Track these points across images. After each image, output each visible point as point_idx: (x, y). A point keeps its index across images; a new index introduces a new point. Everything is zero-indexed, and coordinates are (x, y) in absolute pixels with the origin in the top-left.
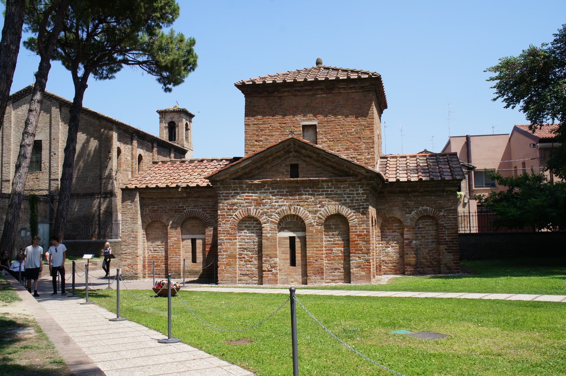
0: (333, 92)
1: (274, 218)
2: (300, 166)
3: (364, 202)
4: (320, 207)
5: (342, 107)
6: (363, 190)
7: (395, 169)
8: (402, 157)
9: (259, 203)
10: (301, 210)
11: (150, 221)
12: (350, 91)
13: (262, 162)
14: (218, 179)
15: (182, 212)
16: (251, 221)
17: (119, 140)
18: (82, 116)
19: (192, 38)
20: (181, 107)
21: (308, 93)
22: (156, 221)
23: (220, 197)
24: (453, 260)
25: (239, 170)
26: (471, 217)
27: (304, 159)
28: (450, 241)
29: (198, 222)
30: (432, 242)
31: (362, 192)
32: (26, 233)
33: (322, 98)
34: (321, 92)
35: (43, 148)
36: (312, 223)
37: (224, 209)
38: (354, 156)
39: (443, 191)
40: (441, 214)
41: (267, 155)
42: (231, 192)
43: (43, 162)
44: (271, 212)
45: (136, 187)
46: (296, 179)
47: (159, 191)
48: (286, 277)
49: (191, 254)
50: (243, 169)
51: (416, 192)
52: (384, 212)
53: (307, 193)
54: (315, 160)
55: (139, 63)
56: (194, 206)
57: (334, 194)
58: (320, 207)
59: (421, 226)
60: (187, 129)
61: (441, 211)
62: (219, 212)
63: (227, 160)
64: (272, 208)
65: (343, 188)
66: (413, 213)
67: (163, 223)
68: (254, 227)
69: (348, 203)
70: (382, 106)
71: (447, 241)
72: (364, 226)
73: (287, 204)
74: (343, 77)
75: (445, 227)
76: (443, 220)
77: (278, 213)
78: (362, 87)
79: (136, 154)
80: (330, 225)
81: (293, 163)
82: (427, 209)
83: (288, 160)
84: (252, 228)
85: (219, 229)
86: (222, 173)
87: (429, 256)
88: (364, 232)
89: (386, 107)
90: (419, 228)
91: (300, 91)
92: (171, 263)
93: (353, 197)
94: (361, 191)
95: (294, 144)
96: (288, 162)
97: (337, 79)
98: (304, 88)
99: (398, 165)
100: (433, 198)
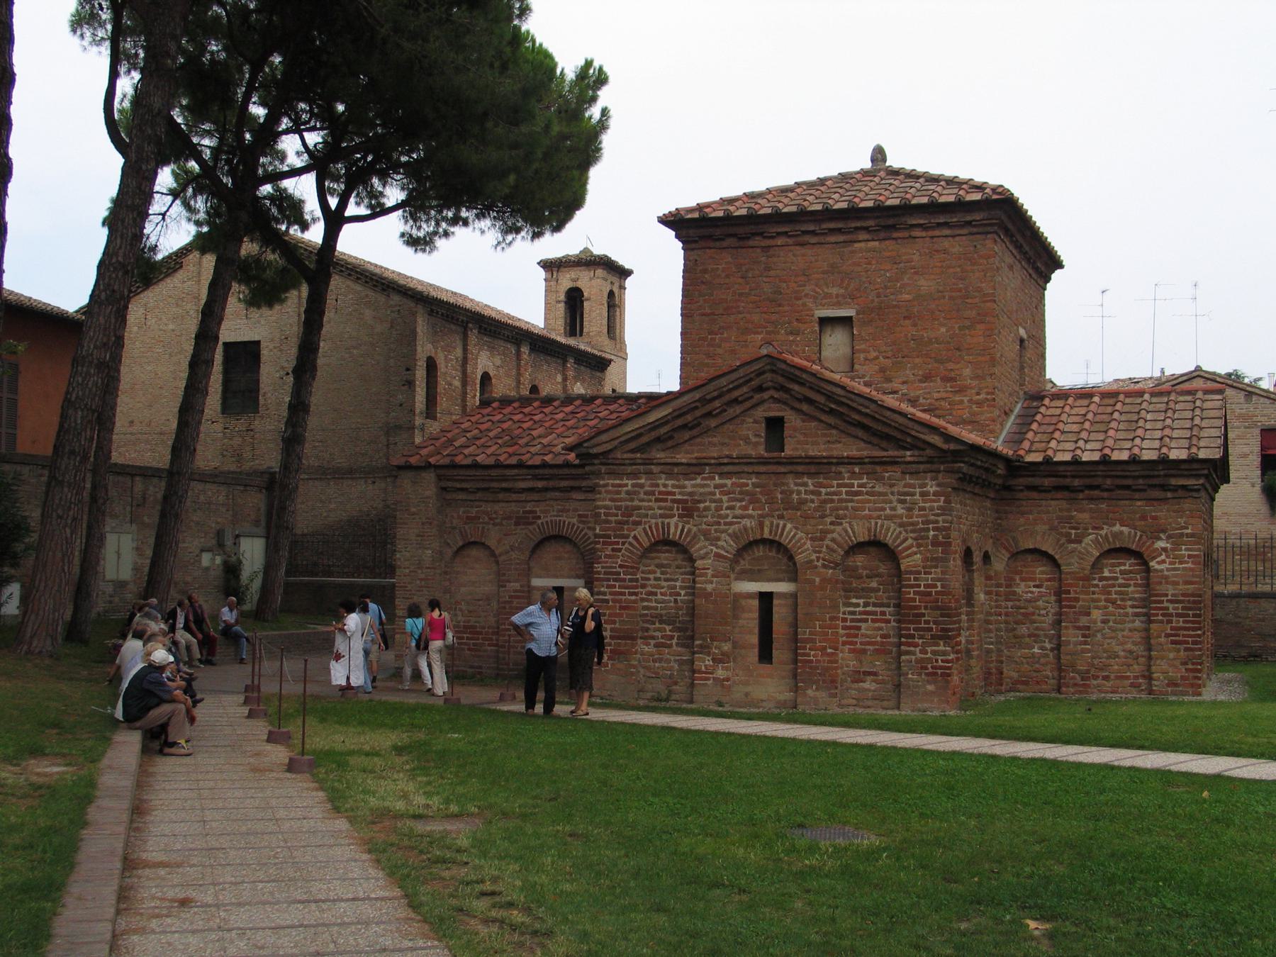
0: (895, 235)
3: (938, 515)
4: (832, 523)
5: (916, 273)
6: (938, 485)
9: (689, 510)
10: (787, 529)
11: (461, 544)
18: (337, 284)
20: (597, 251)
21: (832, 239)
23: (600, 493)
24: (1185, 663)
27: (797, 405)
28: (1178, 615)
29: (568, 547)
30: (1137, 615)
32: (213, 560)
33: (869, 250)
35: (263, 359)
36: (812, 561)
37: (607, 522)
38: (944, 395)
39: (1164, 487)
41: (708, 397)
42: (625, 481)
43: (261, 392)
46: (776, 454)
53: (802, 489)
56: (559, 511)
58: (832, 523)
61: (1160, 539)
64: (719, 523)
65: (889, 478)
67: (488, 548)
69: (901, 517)
71: (1171, 615)
72: (936, 572)
76: (1163, 562)
77: (734, 536)
78: (969, 223)
81: (772, 414)
83: (760, 409)
85: (598, 567)
88: (936, 586)
89: (1056, 263)
91: (813, 233)
94: (932, 488)
96: (761, 413)
100: (1139, 503)
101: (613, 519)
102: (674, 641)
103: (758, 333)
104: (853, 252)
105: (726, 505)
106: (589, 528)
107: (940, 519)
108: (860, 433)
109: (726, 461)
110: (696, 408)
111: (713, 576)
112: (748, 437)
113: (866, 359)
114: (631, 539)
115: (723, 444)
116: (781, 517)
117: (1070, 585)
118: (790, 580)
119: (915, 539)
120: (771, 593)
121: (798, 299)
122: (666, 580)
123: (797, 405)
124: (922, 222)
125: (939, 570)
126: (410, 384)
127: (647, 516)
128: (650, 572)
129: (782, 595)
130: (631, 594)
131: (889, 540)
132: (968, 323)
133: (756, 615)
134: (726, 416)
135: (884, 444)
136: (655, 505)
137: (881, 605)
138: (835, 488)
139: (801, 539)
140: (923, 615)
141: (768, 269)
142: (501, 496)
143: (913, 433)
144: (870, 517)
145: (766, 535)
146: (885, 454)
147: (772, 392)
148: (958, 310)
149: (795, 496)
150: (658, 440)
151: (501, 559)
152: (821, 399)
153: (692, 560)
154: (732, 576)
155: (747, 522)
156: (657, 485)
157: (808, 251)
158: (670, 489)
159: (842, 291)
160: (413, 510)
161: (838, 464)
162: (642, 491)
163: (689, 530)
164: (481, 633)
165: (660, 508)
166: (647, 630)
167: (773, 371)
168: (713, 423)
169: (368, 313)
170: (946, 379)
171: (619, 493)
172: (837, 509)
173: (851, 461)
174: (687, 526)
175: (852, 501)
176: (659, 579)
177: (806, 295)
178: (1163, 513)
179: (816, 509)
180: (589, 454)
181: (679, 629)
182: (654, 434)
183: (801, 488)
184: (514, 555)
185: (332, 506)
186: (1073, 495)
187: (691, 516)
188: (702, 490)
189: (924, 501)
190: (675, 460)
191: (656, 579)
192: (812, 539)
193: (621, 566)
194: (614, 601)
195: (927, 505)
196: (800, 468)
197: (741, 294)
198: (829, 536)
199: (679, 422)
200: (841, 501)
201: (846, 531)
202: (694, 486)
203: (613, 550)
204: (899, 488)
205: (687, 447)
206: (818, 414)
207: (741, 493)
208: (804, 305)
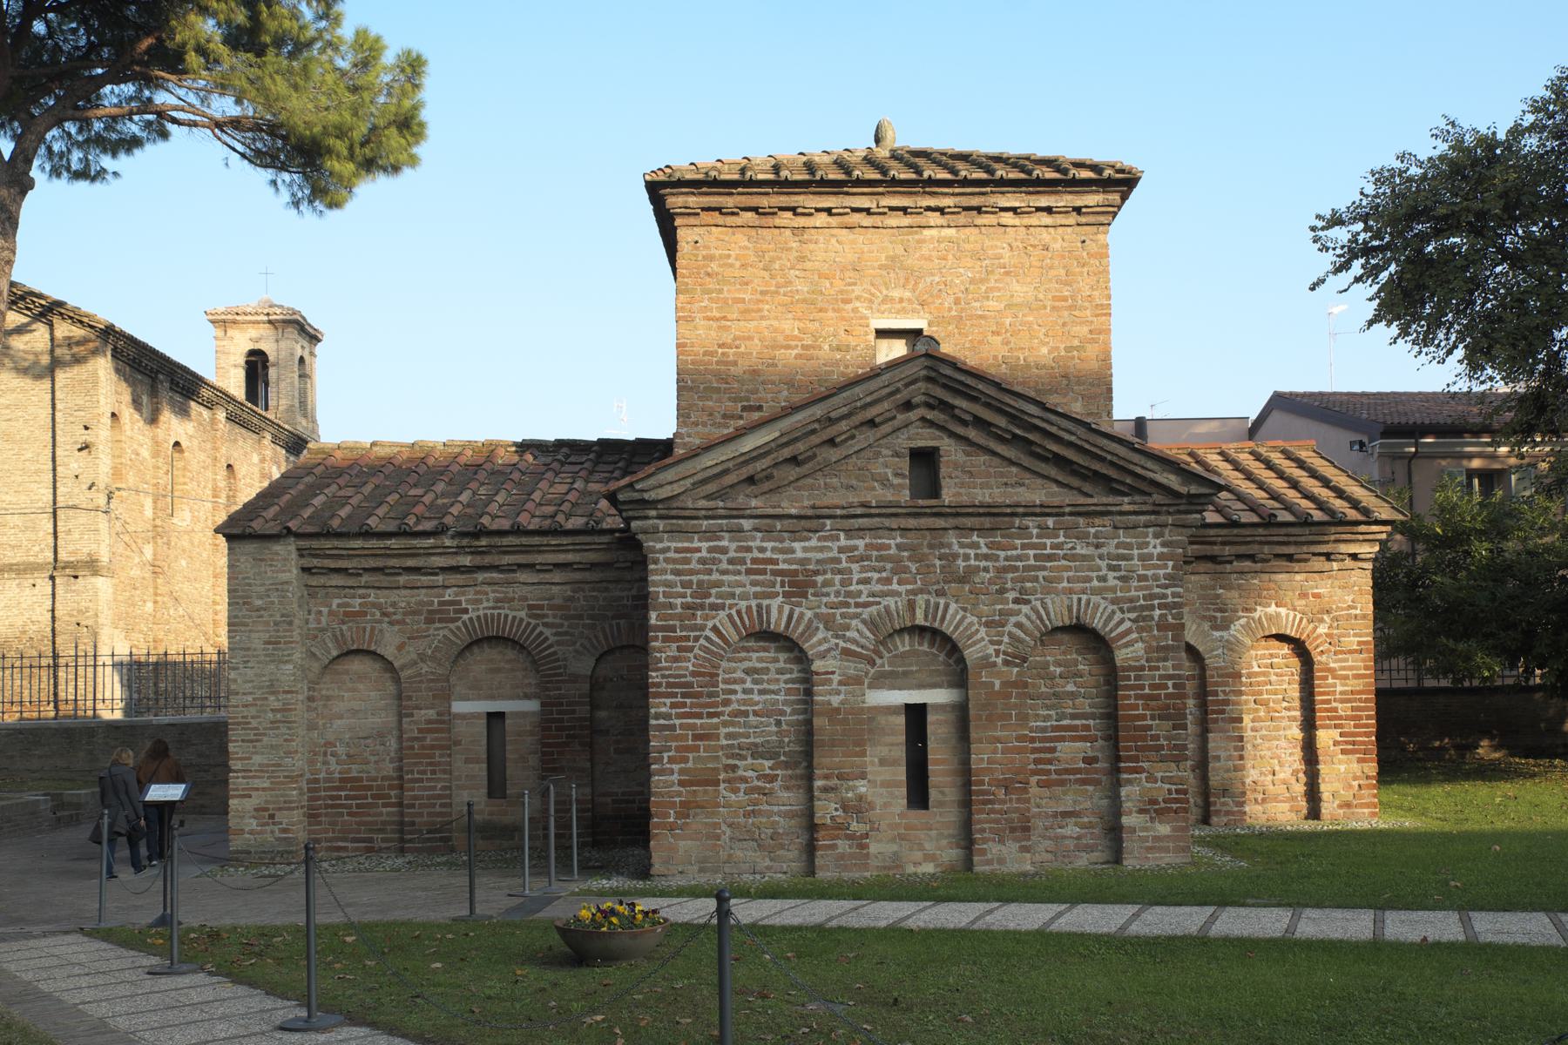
1: (855, 642)
3: (1166, 587)
5: (1007, 273)
6: (1163, 545)
10: (951, 611)
11: (335, 653)
15: (454, 620)
19: (414, 55)
26: (100, 669)
27: (960, 430)
28: (1347, 718)
31: (1159, 549)
36: (987, 657)
37: (671, 606)
40: (1322, 629)
42: (696, 544)
44: (843, 616)
48: (895, 848)
49: (485, 766)
53: (972, 552)
56: (497, 600)
57: (1065, 557)
59: (1256, 669)
61: (1322, 621)
62: (653, 615)
64: (847, 605)
65: (1096, 536)
68: (780, 672)
69: (1113, 589)
71: (1340, 718)
73: (902, 589)
77: (872, 624)
78: (1078, 210)
82: (1278, 615)
92: (415, 798)
94: (1155, 547)
96: (905, 441)
101: (679, 601)
103: (788, 347)
104: (919, 242)
105: (856, 577)
107: (1169, 591)
108: (1053, 472)
109: (859, 511)
110: (814, 432)
111: (840, 683)
112: (889, 480)
114: (708, 633)
115: (850, 487)
116: (940, 593)
117: (1217, 684)
118: (951, 685)
120: (924, 705)
122: (761, 692)
123: (960, 430)
124: (1017, 204)
125: (1169, 664)
127: (733, 595)
128: (735, 682)
129: (939, 708)
130: (711, 715)
131: (1097, 623)
132: (1076, 343)
133: (903, 738)
134: (855, 445)
135: (1087, 488)
138: (1022, 549)
139: (971, 624)
140: (1150, 728)
141: (802, 259)
142: (402, 579)
143: (1139, 470)
144: (1071, 591)
145: (920, 620)
146: (1090, 501)
147: (921, 412)
149: (961, 563)
150: (751, 480)
151: (403, 674)
152: (1002, 422)
153: (801, 658)
155: (890, 602)
156: (749, 549)
157: (859, 237)
158: (768, 554)
159: (908, 294)
160: (259, 602)
161: (1025, 515)
162: (724, 558)
163: (802, 615)
164: (370, 788)
165: (754, 584)
166: (734, 768)
167: (929, 379)
168: (833, 454)
172: (1023, 580)
173: (1044, 511)
174: (797, 610)
175: (1044, 568)
176: (750, 691)
177: (858, 298)
178: (1323, 587)
180: (643, 501)
181: (786, 765)
182: (745, 472)
183: (969, 549)
186: (1219, 568)
188: (820, 556)
189: (1145, 567)
190: (778, 511)
191: (745, 691)
192: (987, 625)
193: (694, 674)
196: (968, 522)
197: (762, 293)
198: (1013, 619)
199: (786, 453)
200: (1027, 568)
202: (805, 549)
203: (679, 649)
204: (1110, 547)
205: (791, 491)
206: (993, 445)
207: (880, 559)
208: (855, 310)
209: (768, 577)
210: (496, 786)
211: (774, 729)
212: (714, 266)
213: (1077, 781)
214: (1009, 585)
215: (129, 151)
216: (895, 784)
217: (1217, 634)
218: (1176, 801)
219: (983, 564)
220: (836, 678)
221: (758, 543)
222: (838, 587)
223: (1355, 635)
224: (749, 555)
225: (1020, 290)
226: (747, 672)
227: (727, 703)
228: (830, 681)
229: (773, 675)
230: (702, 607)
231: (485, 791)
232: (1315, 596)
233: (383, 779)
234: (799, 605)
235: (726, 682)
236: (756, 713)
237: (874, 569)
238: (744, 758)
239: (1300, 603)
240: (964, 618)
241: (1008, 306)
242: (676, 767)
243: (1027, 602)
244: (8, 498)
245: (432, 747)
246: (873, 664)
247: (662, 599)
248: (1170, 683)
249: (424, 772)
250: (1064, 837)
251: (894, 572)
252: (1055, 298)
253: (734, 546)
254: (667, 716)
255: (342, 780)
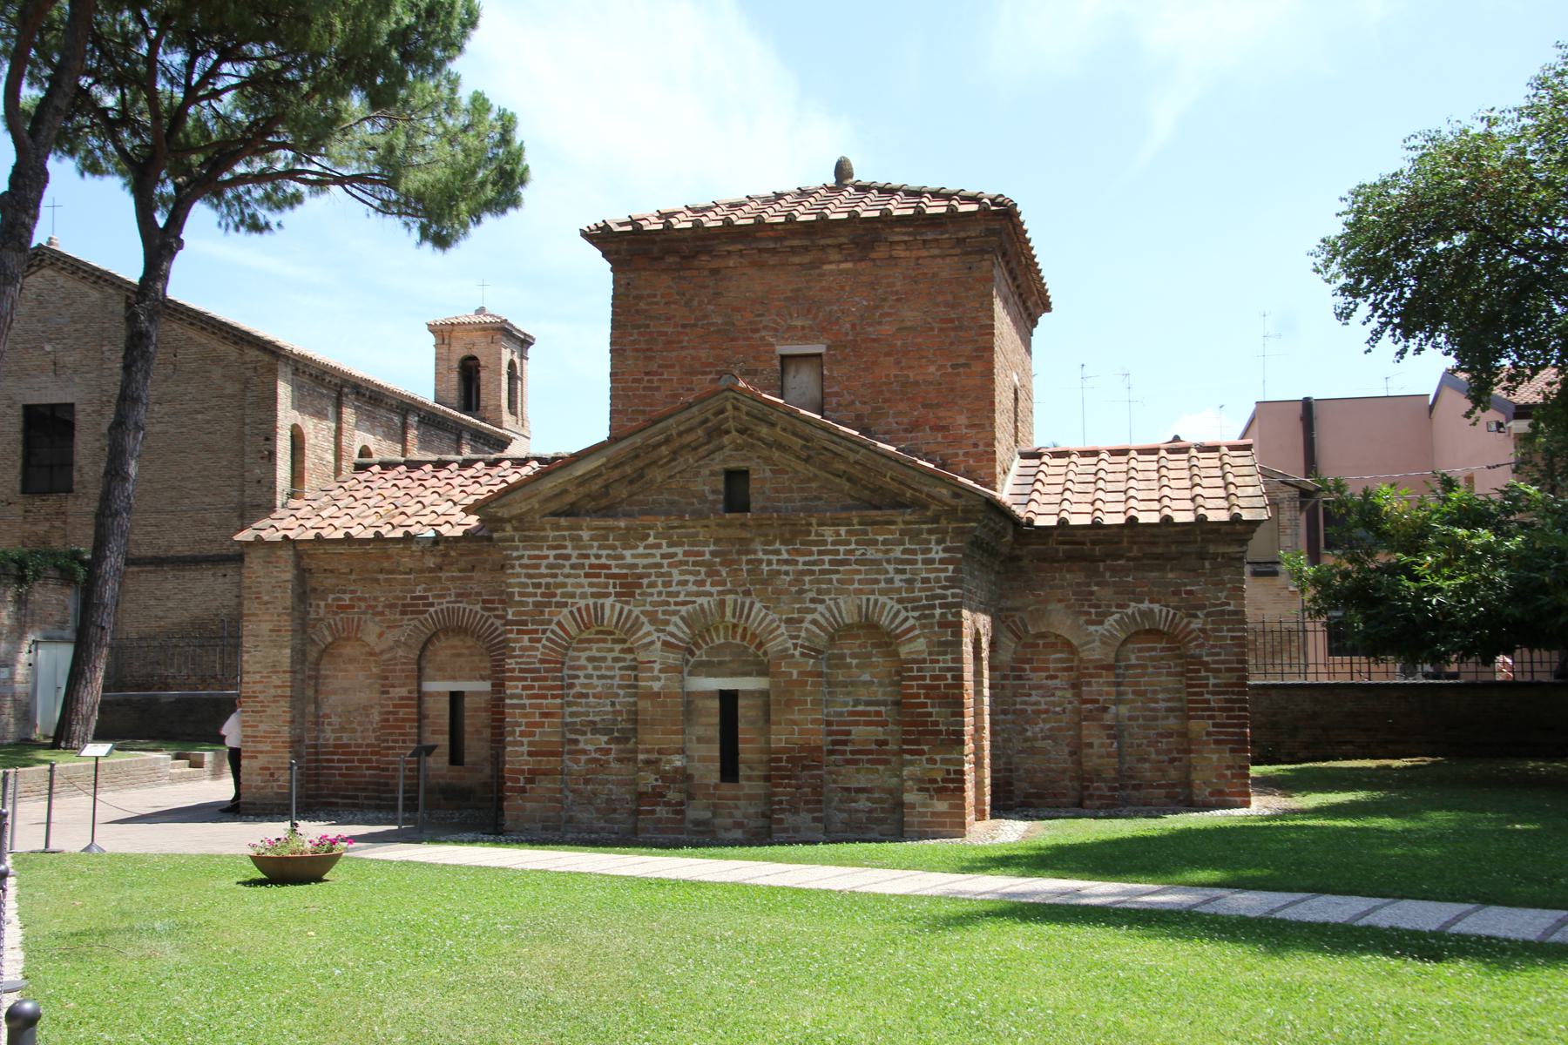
0: (874, 255)
1: (672, 635)
2: (753, 476)
4: (813, 601)
5: (899, 300)
6: (945, 550)
7: (1059, 489)
8: (1084, 454)
9: (629, 586)
10: (755, 610)
12: (924, 253)
13: (639, 464)
14: (503, 513)
16: (604, 641)
17: (299, 405)
21: (797, 260)
22: (348, 639)
23: (513, 567)
25: (571, 488)
27: (766, 453)
28: (1220, 709)
29: (470, 642)
30: (1169, 710)
31: (942, 555)
33: (841, 272)
34: (838, 257)
36: (787, 649)
39: (1202, 556)
40: (1196, 624)
42: (546, 552)
43: (76, 467)
44: (664, 613)
45: (286, 537)
47: (356, 549)
50: (580, 484)
51: (1120, 557)
52: (1021, 619)
53: (774, 558)
54: (798, 457)
55: (341, 181)
56: (458, 595)
57: (857, 562)
58: (813, 601)
59: (1134, 661)
60: (513, 377)
61: (1196, 616)
63: (540, 460)
64: (668, 604)
65: (885, 542)
66: (1111, 620)
68: (616, 660)
69: (899, 590)
70: (1031, 301)
71: (1213, 709)
74: (899, 207)
75: (1205, 664)
76: (1200, 646)
79: (350, 446)
80: (843, 657)
81: (733, 465)
82: (1152, 610)
83: (718, 456)
84: (609, 663)
85: (511, 663)
86: (518, 495)
87: (1158, 752)
89: (1047, 307)
90: (1128, 667)
91: (774, 251)
93: (914, 572)
94: (937, 553)
95: (736, 408)
96: (719, 463)
97: (886, 217)
98: (787, 243)
99: (1071, 476)
100: (1170, 575)
101: (530, 600)
102: (612, 756)
103: (705, 373)
104: (821, 275)
106: (496, 617)
107: (949, 592)
111: (661, 671)
113: (839, 404)
114: (554, 627)
116: (747, 593)
119: (917, 619)
120: (462, 693)
121: (756, 331)
122: (599, 677)
125: (949, 657)
126: (272, 455)
127: (573, 595)
129: (750, 694)
130: (554, 697)
131: (884, 621)
132: (962, 360)
133: (717, 720)
136: (586, 581)
137: (878, 703)
140: (930, 715)
148: (951, 344)
154: (686, 670)
155: (703, 600)
156: (587, 556)
158: (603, 561)
159: (807, 323)
160: (266, 598)
162: (567, 563)
163: (630, 612)
164: (356, 753)
165: (591, 585)
166: (576, 742)
169: (217, 373)
170: (937, 428)
171: (537, 566)
172: (819, 582)
175: (837, 572)
177: (765, 328)
179: (791, 584)
181: (617, 741)
183: (773, 557)
184: (400, 652)
185: (170, 604)
187: (632, 595)
189: (928, 571)
193: (542, 661)
194: (531, 706)
195: (932, 576)
197: (684, 326)
198: (809, 617)
200: (822, 572)
201: (830, 610)
202: (633, 556)
203: (531, 640)
207: (695, 564)
208: (762, 338)
209: (602, 580)
210: (456, 756)
211: (609, 709)
212: (642, 305)
213: (869, 761)
214: (807, 587)
215: (292, 206)
216: (711, 759)
217: (1092, 628)
218: (952, 781)
219: (785, 568)
220: (657, 666)
221: (594, 551)
222: (660, 588)
223: (1229, 630)
224: (587, 562)
225: (910, 315)
226: (590, 659)
227: (571, 686)
228: (651, 670)
229: (609, 663)
230: (549, 604)
231: (447, 758)
232: (1187, 592)
233: (368, 746)
234: (627, 603)
235: (571, 668)
236: (595, 696)
237: (690, 573)
238: (585, 733)
239: (1174, 601)
240: (766, 615)
241: (899, 330)
242: (525, 740)
243: (822, 602)
244: (207, 500)
245: (404, 720)
246: (692, 653)
247: (517, 598)
248: (949, 675)
249: (396, 741)
250: (857, 811)
251: (708, 574)
252: (943, 321)
253: (575, 553)
254: (520, 697)
255: (336, 746)
